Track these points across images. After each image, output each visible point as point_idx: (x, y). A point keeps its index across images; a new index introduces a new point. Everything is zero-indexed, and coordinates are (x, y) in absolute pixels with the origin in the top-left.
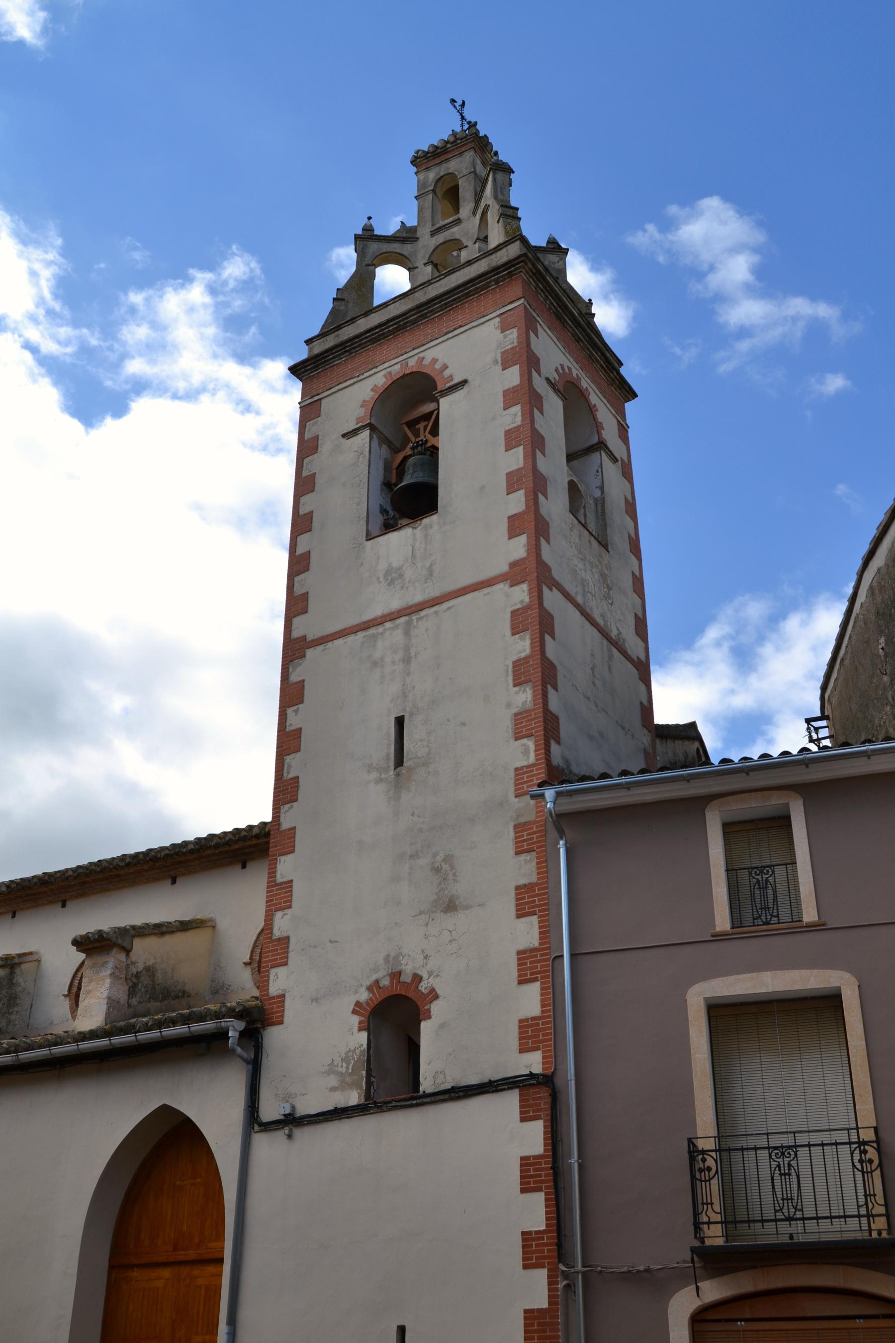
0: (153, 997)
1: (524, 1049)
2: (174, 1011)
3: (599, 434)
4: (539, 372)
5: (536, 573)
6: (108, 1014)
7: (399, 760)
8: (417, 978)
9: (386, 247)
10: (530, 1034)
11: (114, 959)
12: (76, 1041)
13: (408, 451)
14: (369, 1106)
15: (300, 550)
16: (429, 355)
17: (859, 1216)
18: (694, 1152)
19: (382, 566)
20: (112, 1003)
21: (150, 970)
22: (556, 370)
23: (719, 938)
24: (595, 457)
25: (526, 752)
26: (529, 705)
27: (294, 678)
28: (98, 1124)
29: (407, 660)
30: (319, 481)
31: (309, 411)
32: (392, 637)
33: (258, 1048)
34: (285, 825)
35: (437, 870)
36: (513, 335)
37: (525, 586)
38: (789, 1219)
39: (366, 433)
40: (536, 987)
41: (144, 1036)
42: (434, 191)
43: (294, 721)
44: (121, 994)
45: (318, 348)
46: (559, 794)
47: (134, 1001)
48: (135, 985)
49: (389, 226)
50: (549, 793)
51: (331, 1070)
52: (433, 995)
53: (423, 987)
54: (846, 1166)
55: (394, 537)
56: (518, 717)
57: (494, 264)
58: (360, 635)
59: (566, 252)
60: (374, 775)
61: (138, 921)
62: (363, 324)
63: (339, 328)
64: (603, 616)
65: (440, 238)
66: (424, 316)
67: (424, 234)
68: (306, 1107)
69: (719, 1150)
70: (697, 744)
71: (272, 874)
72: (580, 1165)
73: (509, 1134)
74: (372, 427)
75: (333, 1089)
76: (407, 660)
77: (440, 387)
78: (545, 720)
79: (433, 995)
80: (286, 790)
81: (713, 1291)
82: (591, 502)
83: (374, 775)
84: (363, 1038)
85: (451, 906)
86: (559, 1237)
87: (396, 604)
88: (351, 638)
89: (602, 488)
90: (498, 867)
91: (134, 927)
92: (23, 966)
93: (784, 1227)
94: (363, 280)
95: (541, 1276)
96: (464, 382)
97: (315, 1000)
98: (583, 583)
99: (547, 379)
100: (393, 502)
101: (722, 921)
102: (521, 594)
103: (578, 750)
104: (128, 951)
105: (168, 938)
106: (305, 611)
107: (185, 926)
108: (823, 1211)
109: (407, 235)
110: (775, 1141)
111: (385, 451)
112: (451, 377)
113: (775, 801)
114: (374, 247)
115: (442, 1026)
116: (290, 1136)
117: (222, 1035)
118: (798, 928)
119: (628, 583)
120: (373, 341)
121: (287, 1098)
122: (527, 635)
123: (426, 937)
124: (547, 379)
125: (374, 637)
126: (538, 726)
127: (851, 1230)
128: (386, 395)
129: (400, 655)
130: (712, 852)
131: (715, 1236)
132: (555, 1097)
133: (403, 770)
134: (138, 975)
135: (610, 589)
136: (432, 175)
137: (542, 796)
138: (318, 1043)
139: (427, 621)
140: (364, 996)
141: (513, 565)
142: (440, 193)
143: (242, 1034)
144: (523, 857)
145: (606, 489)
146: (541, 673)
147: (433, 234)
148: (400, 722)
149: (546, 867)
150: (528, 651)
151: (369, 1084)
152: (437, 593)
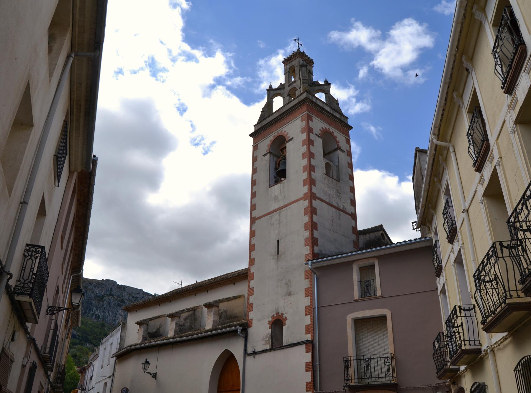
0: (227, 318)
2: (239, 321)
3: (338, 144)
4: (312, 133)
5: (312, 196)
6: (213, 325)
7: (278, 253)
9: (276, 92)
10: (309, 329)
11: (214, 309)
12: (205, 333)
13: (281, 159)
14: (272, 349)
15: (253, 191)
16: (284, 130)
18: (347, 362)
19: (273, 195)
20: (214, 321)
21: (225, 311)
22: (320, 130)
24: (336, 152)
25: (307, 250)
26: (308, 236)
27: (253, 229)
28: (207, 357)
29: (279, 223)
31: (255, 148)
32: (276, 216)
34: (252, 271)
35: (287, 284)
36: (304, 123)
37: (307, 201)
38: (368, 378)
39: (269, 155)
40: (309, 316)
41: (186, 338)
42: (289, 72)
43: (253, 242)
44: (217, 318)
46: (312, 263)
47: (221, 320)
48: (221, 316)
49: (275, 86)
50: (310, 263)
51: (263, 340)
53: (284, 317)
54: (383, 364)
55: (276, 186)
56: (306, 240)
57: (300, 100)
58: (269, 216)
59: (330, 84)
60: (272, 257)
61: (221, 298)
62: (271, 118)
63: (265, 119)
64: (337, 203)
65: (291, 87)
66: (282, 118)
67: (286, 86)
68: (258, 349)
69: (357, 360)
70: (382, 232)
71: (249, 285)
72: (319, 365)
73: (301, 357)
74: (270, 153)
75: (264, 345)
76: (279, 223)
77: (287, 140)
78: (312, 240)
80: (252, 262)
82: (335, 167)
83: (272, 257)
84: (270, 331)
85: (290, 294)
86: (314, 383)
87: (277, 207)
88: (266, 217)
89: (338, 162)
90: (300, 283)
91: (219, 300)
93: (367, 380)
94: (269, 105)
96: (293, 138)
97: (259, 320)
98: (329, 195)
99: (316, 135)
100: (276, 174)
101: (356, 296)
103: (324, 246)
104: (218, 307)
105: (230, 302)
106: (255, 209)
107: (235, 298)
108: (377, 376)
109: (282, 87)
111: (275, 158)
112: (289, 137)
114: (272, 92)
115: (288, 327)
116: (254, 357)
117: (236, 331)
118: (376, 298)
119: (348, 189)
120: (270, 126)
121: (253, 347)
122: (308, 216)
123: (284, 303)
124: (316, 135)
125: (271, 216)
126: (310, 242)
127: (383, 381)
128: (273, 143)
130: (354, 277)
131: (353, 383)
132: (313, 346)
133: (279, 255)
134: (221, 313)
135: (340, 194)
136: (288, 67)
137: (308, 264)
138: (260, 332)
139: (284, 211)
140: (270, 319)
141: (305, 194)
142: (291, 72)
143: (242, 330)
144: (307, 280)
145: (340, 162)
146: (313, 226)
147: (289, 86)
148: (278, 241)
149: (312, 282)
150: (308, 221)
151: (272, 343)
152: (286, 203)
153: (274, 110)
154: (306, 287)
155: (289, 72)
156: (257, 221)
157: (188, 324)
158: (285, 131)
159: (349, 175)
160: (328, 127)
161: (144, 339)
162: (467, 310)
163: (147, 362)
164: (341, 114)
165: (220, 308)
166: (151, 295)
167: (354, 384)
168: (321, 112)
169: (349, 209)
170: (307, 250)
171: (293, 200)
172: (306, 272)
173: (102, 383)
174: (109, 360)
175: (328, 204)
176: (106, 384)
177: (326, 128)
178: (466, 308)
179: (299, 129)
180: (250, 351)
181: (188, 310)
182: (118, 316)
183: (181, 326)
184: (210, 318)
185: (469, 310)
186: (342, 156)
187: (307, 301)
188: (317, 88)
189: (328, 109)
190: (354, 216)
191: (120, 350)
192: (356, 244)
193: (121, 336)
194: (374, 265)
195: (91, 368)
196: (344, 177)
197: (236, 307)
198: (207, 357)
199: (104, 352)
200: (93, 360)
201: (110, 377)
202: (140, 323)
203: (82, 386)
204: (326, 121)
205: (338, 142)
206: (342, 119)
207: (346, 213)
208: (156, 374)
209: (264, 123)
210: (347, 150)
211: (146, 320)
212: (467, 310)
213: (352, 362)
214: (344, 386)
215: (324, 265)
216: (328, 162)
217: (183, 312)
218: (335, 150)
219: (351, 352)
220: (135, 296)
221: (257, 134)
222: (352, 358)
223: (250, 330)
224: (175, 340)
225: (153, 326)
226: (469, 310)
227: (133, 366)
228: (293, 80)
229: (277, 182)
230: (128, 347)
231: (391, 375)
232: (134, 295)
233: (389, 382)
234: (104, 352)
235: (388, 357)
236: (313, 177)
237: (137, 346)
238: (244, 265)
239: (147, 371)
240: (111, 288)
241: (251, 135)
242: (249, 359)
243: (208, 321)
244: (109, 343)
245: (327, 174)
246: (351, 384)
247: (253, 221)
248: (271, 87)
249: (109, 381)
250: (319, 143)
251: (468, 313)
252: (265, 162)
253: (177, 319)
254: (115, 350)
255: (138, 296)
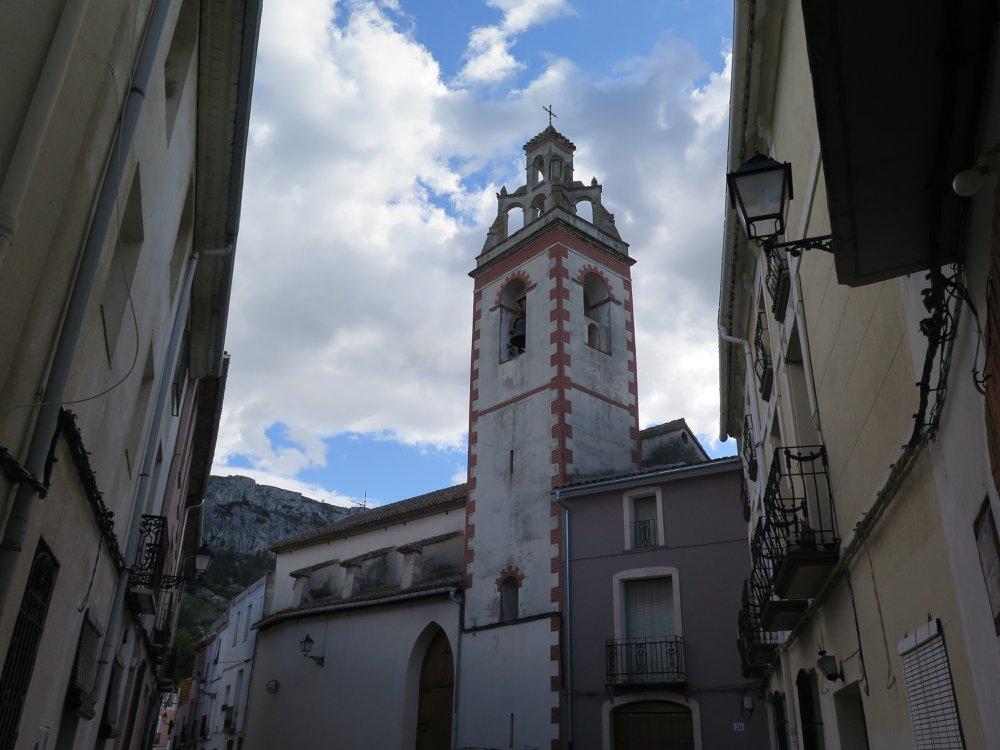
1: (553, 601)
8: (517, 569)
10: (557, 594)
11: (413, 557)
17: (652, 673)
18: (611, 647)
23: (626, 553)
28: (401, 632)
29: (514, 424)
30: (481, 332)
31: (478, 296)
32: (509, 411)
33: (463, 597)
39: (499, 309)
41: (370, 602)
42: (534, 165)
43: (474, 451)
45: (485, 260)
49: (511, 191)
52: (523, 577)
53: (519, 573)
54: (664, 650)
58: (498, 411)
65: (536, 193)
68: (482, 622)
73: (543, 636)
74: (502, 306)
76: (514, 424)
79: (523, 577)
81: (620, 701)
82: (604, 330)
87: (510, 397)
89: (609, 322)
90: (544, 521)
92: (390, 554)
93: (640, 676)
95: (557, 694)
100: (511, 341)
101: (628, 546)
102: (554, 395)
107: (449, 537)
109: (522, 191)
110: (639, 641)
111: (510, 316)
113: (650, 491)
117: (448, 593)
118: (656, 548)
119: (625, 365)
121: (474, 620)
124: (573, 279)
127: (658, 679)
129: (511, 422)
131: (620, 680)
132: (562, 621)
136: (533, 157)
138: (483, 594)
140: (499, 576)
141: (553, 379)
146: (562, 431)
148: (512, 452)
152: (525, 392)
153: (510, 233)
154: (554, 528)
155: (535, 165)
156: (480, 419)
157: (373, 577)
158: (524, 273)
159: (628, 342)
160: (593, 264)
161: (304, 600)
162: (806, 459)
163: (308, 640)
164: (618, 239)
165: (424, 554)
166: (316, 502)
167: (621, 682)
168: (582, 239)
169: (627, 399)
170: (553, 470)
171: (535, 387)
172: (553, 504)
173: (235, 671)
174: (246, 636)
175: (592, 393)
176: (241, 671)
177: (590, 266)
178: (806, 453)
179: (545, 271)
180: (468, 625)
181: (374, 555)
182: (258, 539)
183: (364, 580)
184: (408, 562)
185: (812, 457)
186: (616, 311)
187: (554, 551)
188: (579, 193)
189: (594, 233)
190: (634, 410)
191: (264, 617)
192: (635, 455)
193: (266, 594)
194: (655, 497)
195: (215, 643)
196: (619, 346)
197: (448, 552)
198: (401, 632)
199: (238, 620)
200: (219, 630)
201: (247, 661)
202: (296, 575)
203: (199, 674)
204: (588, 254)
205: (611, 287)
206: (619, 249)
207: (621, 405)
208: (322, 659)
209: (493, 255)
210: (626, 301)
211: (305, 570)
212: (806, 459)
213: (619, 648)
214: (606, 685)
215: (578, 494)
216: (593, 322)
217: (365, 557)
218: (607, 301)
219: (618, 634)
220: (288, 504)
221: (481, 274)
222: (619, 642)
223: (469, 593)
224: (352, 604)
225: (320, 577)
226: (812, 457)
227: (289, 641)
228: (541, 178)
229: (512, 355)
230: (278, 613)
231: (675, 670)
232: (285, 502)
233: (672, 681)
234: (238, 620)
235: (671, 642)
236: (567, 351)
237: (292, 613)
238: (461, 478)
239: (309, 654)
240: (245, 492)
241: (471, 274)
242: (467, 638)
243: (406, 574)
244: (246, 603)
245: (591, 343)
246: (618, 682)
247: (474, 416)
248: (504, 190)
249: (247, 668)
250: (577, 293)
251: (807, 466)
252: (492, 319)
253: (355, 569)
254: (256, 617)
255: (293, 504)
